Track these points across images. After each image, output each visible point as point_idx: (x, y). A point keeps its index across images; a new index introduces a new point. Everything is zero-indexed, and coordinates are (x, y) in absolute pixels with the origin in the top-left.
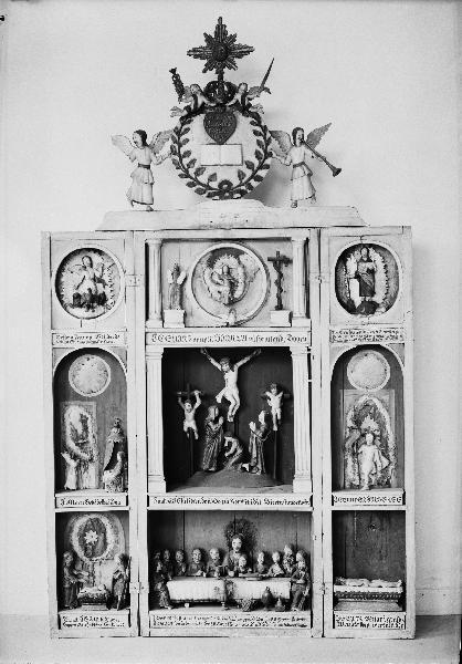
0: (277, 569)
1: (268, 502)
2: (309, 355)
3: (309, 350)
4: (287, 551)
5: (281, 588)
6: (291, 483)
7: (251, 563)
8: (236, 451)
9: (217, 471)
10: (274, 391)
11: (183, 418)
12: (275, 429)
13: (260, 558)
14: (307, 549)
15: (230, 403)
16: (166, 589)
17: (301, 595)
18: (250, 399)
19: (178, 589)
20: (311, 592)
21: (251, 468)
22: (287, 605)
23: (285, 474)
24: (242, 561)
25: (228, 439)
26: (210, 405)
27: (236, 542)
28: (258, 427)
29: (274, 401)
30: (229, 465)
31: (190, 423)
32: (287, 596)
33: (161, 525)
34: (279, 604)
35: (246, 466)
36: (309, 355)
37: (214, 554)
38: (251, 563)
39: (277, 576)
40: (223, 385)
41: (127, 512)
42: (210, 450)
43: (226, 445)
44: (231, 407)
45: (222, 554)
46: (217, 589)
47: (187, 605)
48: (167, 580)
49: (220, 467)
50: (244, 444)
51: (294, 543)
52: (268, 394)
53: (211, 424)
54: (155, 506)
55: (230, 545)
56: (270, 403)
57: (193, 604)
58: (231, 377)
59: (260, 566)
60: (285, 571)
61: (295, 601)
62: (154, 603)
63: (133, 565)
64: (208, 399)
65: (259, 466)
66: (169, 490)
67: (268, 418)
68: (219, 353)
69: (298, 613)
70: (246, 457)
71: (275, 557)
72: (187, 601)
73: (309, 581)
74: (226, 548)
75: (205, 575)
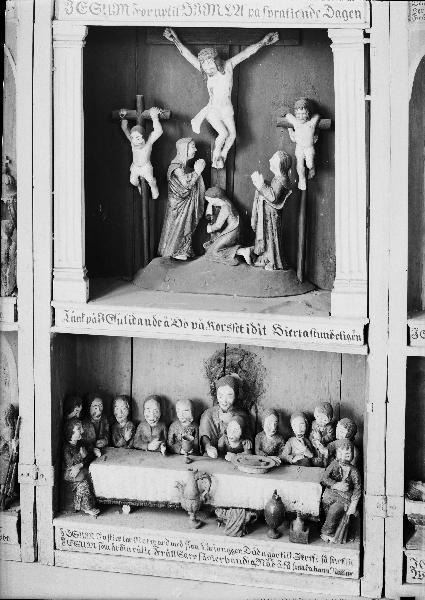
0: (297, 448)
1: (277, 329)
2: (367, 47)
3: (367, 35)
4: (321, 419)
5: (303, 493)
6: (263, 430)
7: (251, 428)
8: (226, 224)
9: (190, 259)
10: (301, 113)
11: (129, 158)
12: (302, 186)
13: (269, 423)
14: (358, 412)
15: (215, 134)
16: (88, 478)
17: (341, 513)
18: (257, 126)
19: (110, 477)
20: (360, 506)
21: (254, 257)
22: (313, 528)
23: (320, 270)
24: (233, 429)
25: (213, 201)
26: (182, 135)
27: (226, 394)
28: (268, 183)
29: (303, 135)
30: (213, 249)
31: (141, 169)
32: (315, 511)
33: (81, 367)
34: (297, 524)
35: (245, 252)
36: (367, 47)
37: (183, 412)
38: (251, 428)
39: (299, 463)
40: (205, 99)
41: (16, 333)
42: (177, 221)
43: (209, 211)
44: (219, 141)
45: (198, 409)
46: (180, 486)
47: (126, 509)
48: (91, 458)
49: (197, 251)
50: (242, 211)
51: (335, 399)
52: (290, 118)
53: (179, 172)
54: (64, 327)
55: (214, 392)
56: (294, 136)
57: (137, 507)
58: (220, 84)
59: (268, 437)
60: (313, 449)
61: (329, 522)
62: (62, 503)
63: (25, 429)
64: (177, 122)
65: (269, 255)
66: (93, 295)
67: (288, 165)
68: (193, 37)
69: (333, 551)
70: (245, 236)
71: (298, 425)
72: (125, 501)
73: (357, 485)
74: (208, 399)
75: (163, 449)
